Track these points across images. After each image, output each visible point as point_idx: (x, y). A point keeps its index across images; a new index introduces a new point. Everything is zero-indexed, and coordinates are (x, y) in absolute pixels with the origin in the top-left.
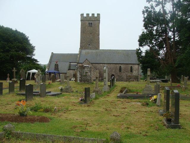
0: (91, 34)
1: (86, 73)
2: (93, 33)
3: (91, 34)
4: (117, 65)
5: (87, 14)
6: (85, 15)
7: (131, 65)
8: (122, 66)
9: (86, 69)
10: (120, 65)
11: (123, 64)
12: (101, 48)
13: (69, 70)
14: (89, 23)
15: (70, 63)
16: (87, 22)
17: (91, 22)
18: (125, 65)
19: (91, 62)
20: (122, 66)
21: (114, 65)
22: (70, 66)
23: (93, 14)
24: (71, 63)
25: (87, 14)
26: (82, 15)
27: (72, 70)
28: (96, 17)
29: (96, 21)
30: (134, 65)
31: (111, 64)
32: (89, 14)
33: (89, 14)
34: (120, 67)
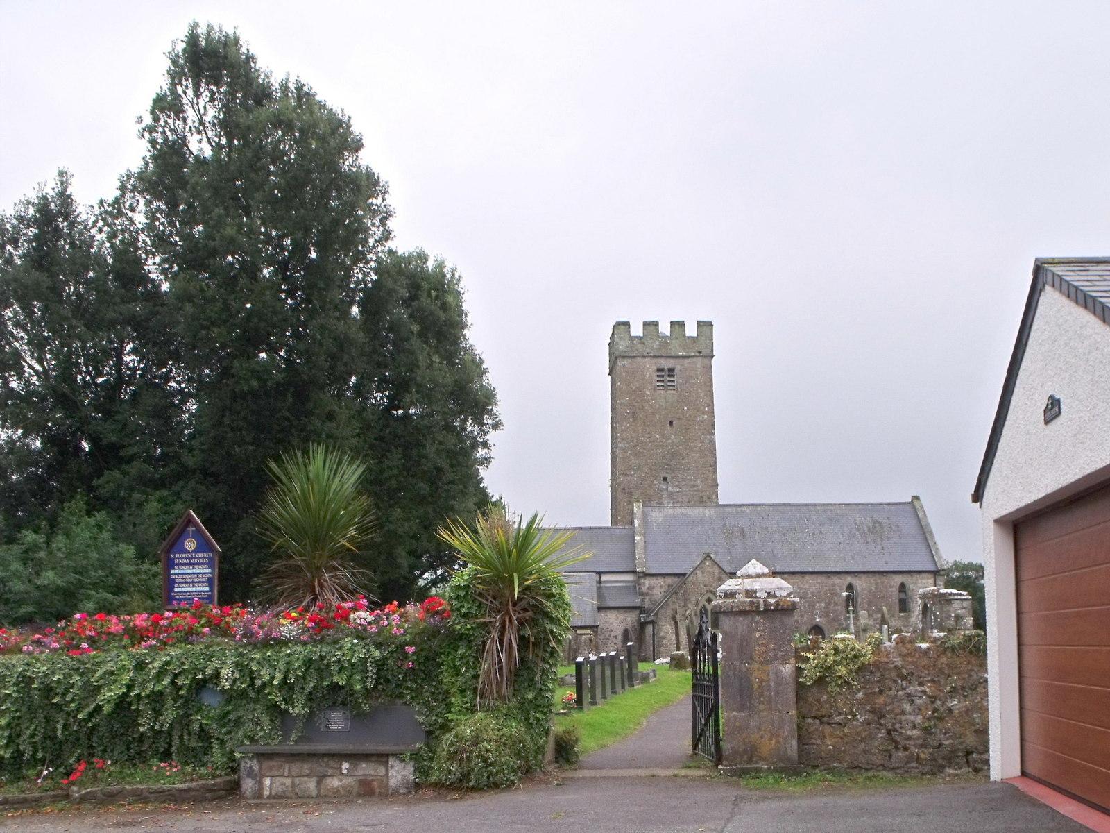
0: (671, 423)
3: (671, 423)
4: (836, 580)
5: (646, 324)
6: (637, 330)
7: (898, 579)
8: (858, 583)
9: (956, 605)
10: (849, 579)
11: (864, 572)
12: (726, 494)
13: (600, 609)
14: (659, 370)
15: (600, 573)
16: (650, 367)
18: (872, 579)
19: (727, 571)
20: (858, 583)
21: (820, 579)
23: (678, 325)
24: (604, 578)
25: (646, 324)
26: (195, 26)
27: (616, 613)
29: (694, 359)
30: (916, 576)
31: (807, 577)
32: (656, 324)
33: (656, 324)
34: (902, 588)
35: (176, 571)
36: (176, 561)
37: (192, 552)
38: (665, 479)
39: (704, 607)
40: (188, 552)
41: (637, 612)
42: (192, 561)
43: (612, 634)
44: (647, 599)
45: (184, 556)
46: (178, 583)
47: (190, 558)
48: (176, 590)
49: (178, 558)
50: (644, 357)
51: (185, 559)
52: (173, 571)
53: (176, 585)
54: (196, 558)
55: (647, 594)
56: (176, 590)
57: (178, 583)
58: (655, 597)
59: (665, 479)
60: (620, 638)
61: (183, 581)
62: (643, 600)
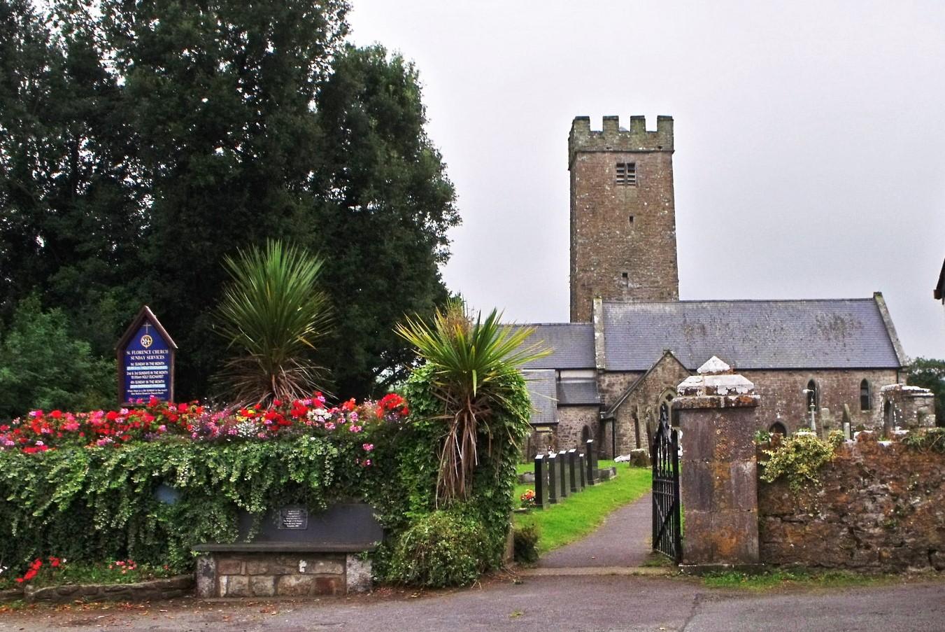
0: (631, 219)
1: (921, 415)
2: (639, 214)
3: (631, 219)
4: (798, 377)
6: (596, 125)
7: (860, 376)
8: (820, 380)
9: (918, 402)
10: (811, 376)
11: (826, 369)
12: (687, 291)
15: (559, 370)
17: (626, 159)
18: (833, 376)
20: (820, 380)
21: (782, 376)
22: (560, 387)
24: (564, 375)
28: (654, 135)
29: (655, 155)
30: (878, 374)
31: (768, 374)
32: (616, 119)
33: (616, 119)
34: (865, 385)
35: (132, 368)
36: (132, 358)
37: (149, 348)
38: (625, 275)
39: (664, 404)
40: (144, 349)
41: (597, 409)
42: (148, 358)
43: (572, 431)
44: (607, 396)
45: (140, 352)
46: (134, 380)
47: (146, 355)
48: (132, 387)
49: (134, 355)
50: (604, 152)
51: (141, 355)
52: (129, 368)
53: (132, 382)
54: (152, 354)
55: (607, 391)
56: (132, 387)
57: (134, 380)
58: (615, 394)
59: (625, 275)
60: (579, 435)
61: (140, 377)
62: (603, 397)
